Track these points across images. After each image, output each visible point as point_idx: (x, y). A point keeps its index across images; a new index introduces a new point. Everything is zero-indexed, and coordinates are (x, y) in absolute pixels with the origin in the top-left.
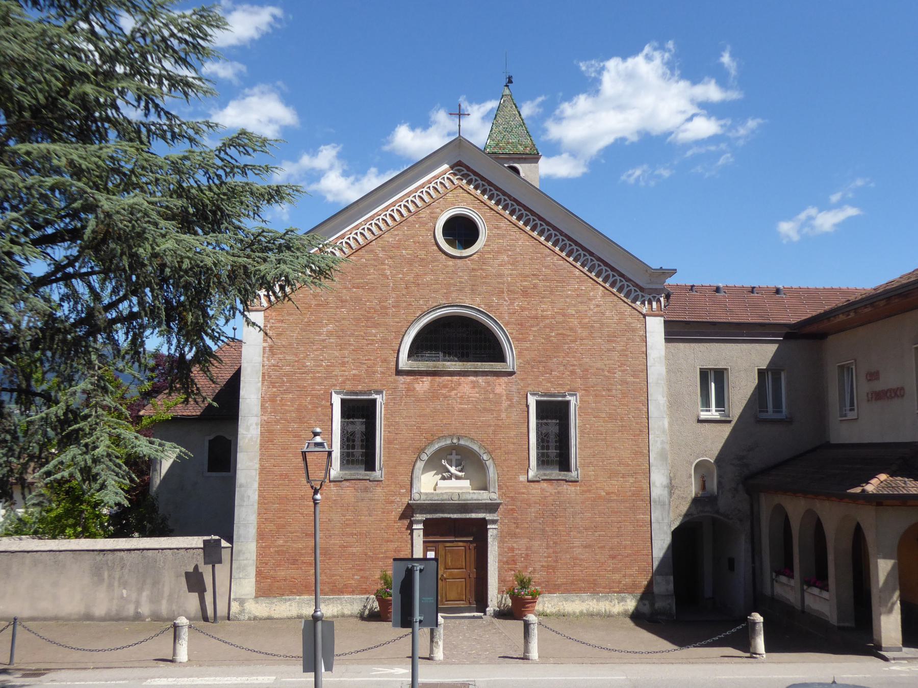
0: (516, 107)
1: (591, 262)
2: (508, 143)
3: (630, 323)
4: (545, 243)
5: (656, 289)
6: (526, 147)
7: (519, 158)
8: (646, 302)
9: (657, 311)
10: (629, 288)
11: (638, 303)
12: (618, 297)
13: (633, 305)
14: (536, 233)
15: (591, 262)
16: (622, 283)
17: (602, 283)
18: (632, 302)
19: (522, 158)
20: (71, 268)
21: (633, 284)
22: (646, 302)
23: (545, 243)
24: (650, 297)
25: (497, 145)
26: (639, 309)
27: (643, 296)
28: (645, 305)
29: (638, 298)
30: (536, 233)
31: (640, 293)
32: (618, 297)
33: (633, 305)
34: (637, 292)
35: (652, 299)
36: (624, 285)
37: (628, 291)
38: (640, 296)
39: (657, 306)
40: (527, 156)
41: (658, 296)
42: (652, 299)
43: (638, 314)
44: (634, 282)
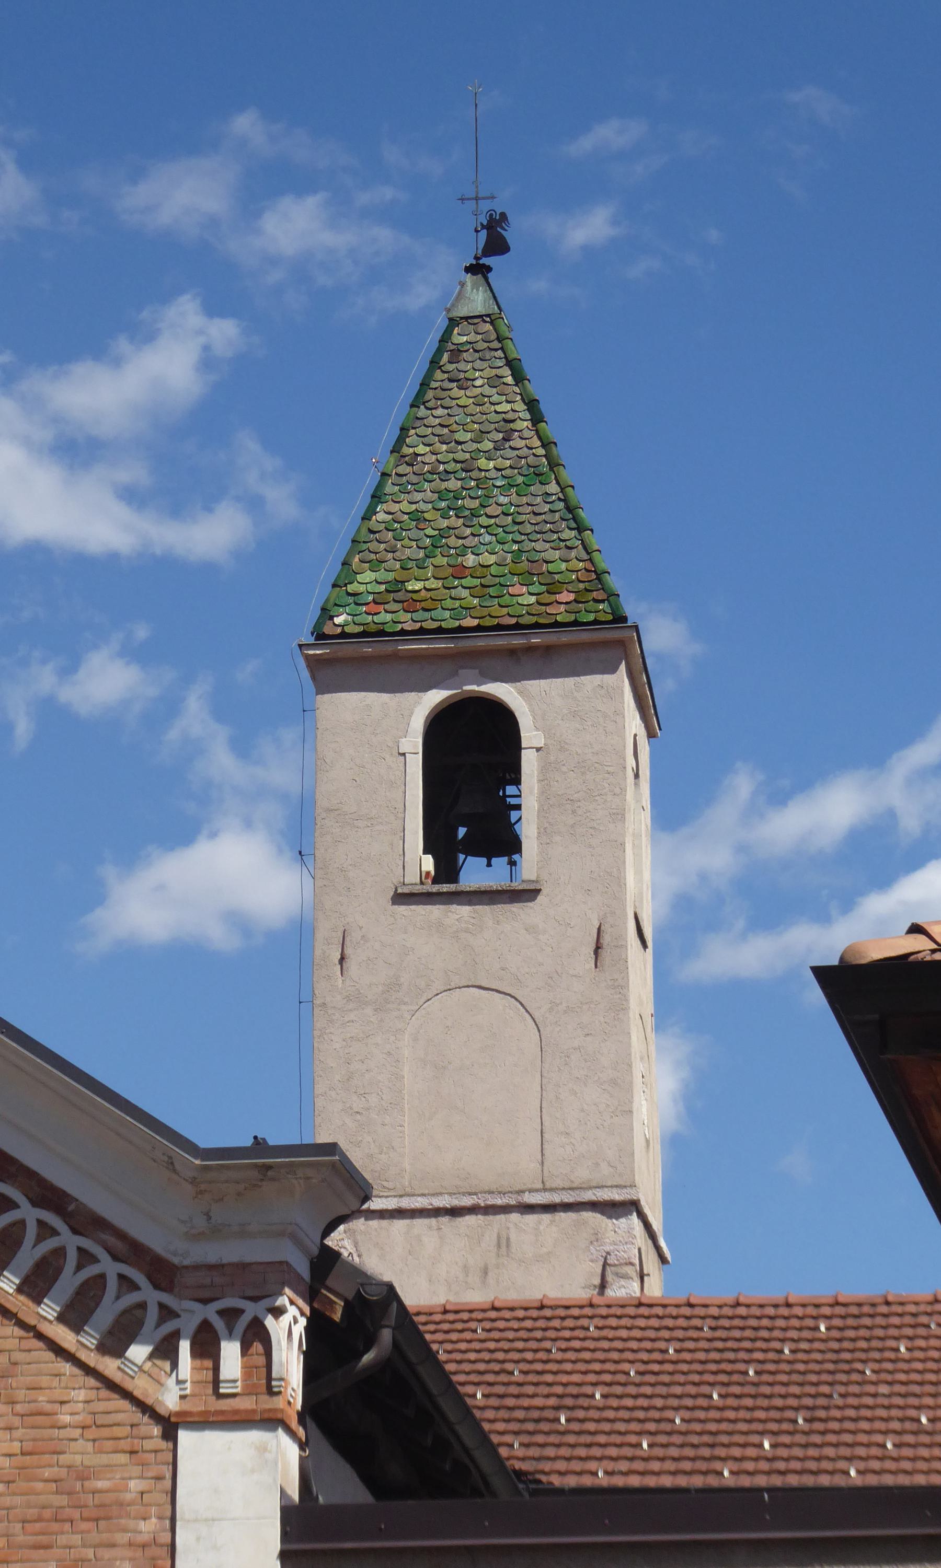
0: (519, 378)
1: (40, 1239)
2: (459, 572)
3: (84, 1475)
4: (65, 1336)
5: (243, 1267)
6: (553, 588)
7: (512, 652)
8: (185, 1347)
9: (249, 1391)
10: (91, 1271)
11: (138, 1352)
12: (22, 1324)
13: (109, 1366)
14: (49, 1310)
15: (40, 1239)
16: (51, 1244)
17: (91, 1358)
18: (103, 1349)
19: (530, 649)
20: (595, 577)
21: (111, 1240)
22: (185, 1347)
23: (65, 1336)
24: (210, 1312)
25: (396, 586)
26: (140, 1386)
27: (167, 1313)
28: (175, 1365)
29: (141, 1323)
30: (49, 1310)
31: (150, 1295)
32: (22, 1324)
33: (109, 1366)
34: (136, 1287)
35: (219, 1324)
36: (60, 1252)
37: (85, 1285)
38: (153, 1313)
39: (248, 1370)
40: (565, 637)
41: (251, 1309)
42: (219, 1324)
43: (138, 1417)
44: (121, 1235)
